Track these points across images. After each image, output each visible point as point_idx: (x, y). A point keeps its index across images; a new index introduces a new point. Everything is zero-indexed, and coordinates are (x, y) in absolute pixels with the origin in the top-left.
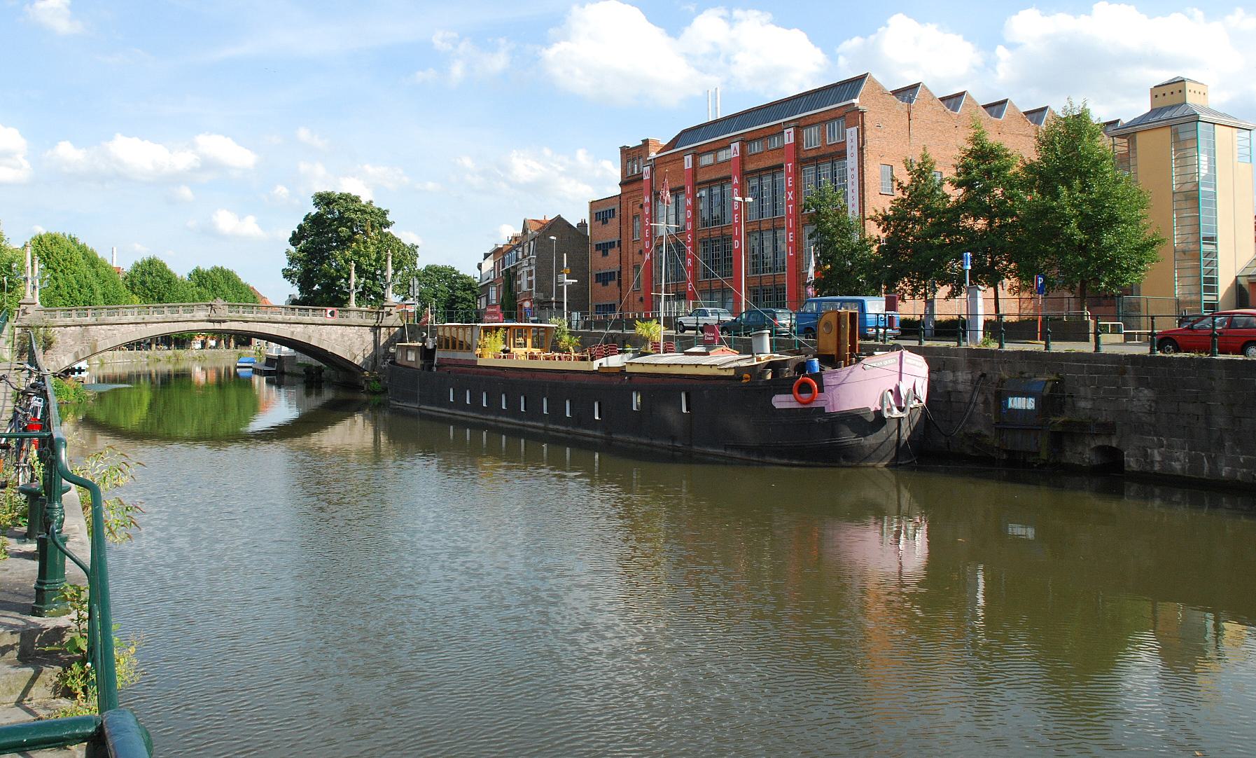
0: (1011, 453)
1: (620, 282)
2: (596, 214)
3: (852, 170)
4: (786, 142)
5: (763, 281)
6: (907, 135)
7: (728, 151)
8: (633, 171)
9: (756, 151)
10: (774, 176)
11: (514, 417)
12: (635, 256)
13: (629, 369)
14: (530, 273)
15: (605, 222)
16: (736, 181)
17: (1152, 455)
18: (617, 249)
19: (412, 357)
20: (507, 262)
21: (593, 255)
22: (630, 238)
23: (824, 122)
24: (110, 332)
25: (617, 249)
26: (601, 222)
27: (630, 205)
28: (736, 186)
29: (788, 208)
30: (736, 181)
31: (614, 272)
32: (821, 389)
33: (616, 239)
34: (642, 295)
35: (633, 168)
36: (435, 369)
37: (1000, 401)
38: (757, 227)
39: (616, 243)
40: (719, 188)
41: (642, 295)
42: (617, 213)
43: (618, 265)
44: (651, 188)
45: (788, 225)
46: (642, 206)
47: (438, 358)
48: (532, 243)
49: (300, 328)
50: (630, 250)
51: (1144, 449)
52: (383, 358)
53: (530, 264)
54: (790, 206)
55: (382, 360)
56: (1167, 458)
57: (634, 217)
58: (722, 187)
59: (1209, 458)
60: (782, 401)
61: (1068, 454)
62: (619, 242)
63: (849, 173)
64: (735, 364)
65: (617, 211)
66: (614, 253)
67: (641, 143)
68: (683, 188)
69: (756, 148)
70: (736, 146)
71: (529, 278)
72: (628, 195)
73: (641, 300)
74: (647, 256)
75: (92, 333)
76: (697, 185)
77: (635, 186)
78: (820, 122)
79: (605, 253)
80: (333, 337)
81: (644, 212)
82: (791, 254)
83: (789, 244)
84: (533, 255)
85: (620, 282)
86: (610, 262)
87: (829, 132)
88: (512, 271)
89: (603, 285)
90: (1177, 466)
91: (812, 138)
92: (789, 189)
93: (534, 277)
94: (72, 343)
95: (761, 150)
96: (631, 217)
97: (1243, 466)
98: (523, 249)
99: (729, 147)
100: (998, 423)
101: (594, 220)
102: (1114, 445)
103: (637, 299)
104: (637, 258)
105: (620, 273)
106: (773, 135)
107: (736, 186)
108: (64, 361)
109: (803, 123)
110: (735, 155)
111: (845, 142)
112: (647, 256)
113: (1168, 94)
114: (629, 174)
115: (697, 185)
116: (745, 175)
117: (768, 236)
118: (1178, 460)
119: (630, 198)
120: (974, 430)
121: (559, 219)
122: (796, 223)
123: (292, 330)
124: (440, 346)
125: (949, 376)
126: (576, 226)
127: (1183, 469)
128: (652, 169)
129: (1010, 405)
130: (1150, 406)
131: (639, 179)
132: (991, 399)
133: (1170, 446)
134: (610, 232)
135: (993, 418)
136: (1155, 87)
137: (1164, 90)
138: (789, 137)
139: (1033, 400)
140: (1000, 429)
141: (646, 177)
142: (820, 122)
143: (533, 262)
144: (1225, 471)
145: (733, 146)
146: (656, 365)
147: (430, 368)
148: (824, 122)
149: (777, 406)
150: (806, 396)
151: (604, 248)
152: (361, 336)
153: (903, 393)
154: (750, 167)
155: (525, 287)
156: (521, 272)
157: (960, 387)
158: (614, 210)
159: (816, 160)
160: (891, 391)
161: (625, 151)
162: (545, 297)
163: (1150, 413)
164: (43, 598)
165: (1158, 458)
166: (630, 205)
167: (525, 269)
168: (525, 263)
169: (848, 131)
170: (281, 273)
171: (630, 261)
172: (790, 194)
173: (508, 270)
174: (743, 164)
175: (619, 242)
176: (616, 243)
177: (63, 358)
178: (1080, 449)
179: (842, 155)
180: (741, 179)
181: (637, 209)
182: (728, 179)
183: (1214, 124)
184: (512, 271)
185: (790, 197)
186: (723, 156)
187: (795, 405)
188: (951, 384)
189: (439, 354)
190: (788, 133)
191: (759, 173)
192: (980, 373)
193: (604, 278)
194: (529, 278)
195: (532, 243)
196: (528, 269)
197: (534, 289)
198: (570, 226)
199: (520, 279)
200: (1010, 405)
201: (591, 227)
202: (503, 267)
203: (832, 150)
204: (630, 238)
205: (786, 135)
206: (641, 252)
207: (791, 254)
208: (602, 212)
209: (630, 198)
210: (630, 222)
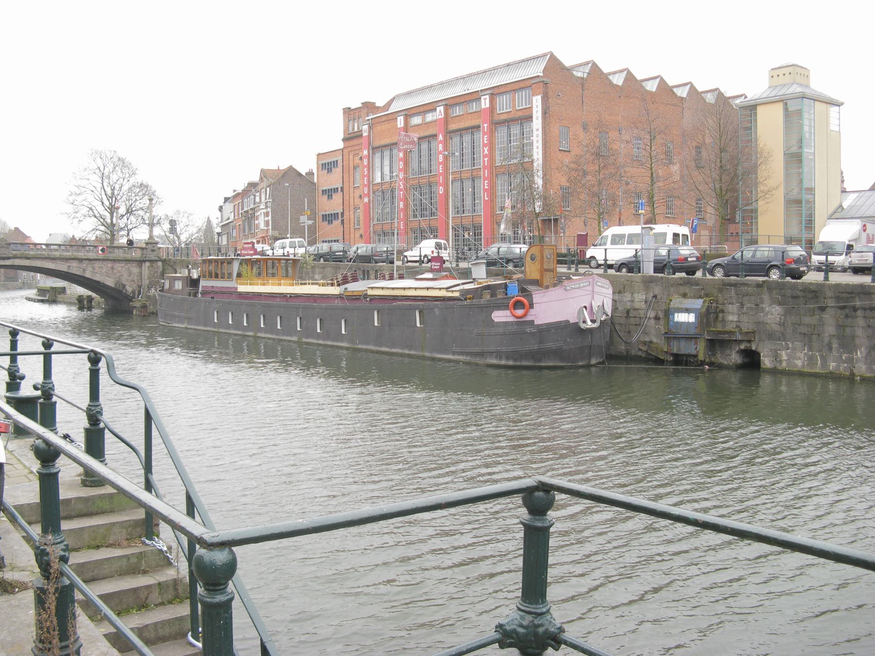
0: (676, 356)
1: (343, 221)
3: (537, 130)
4: (483, 107)
5: (463, 221)
6: (581, 103)
7: (434, 114)
8: (353, 129)
9: (458, 114)
10: (472, 134)
11: (272, 333)
12: (356, 201)
13: (370, 292)
14: (267, 214)
15: (329, 171)
16: (441, 138)
17: (781, 355)
18: (340, 194)
19: (179, 285)
20: (245, 205)
21: (320, 199)
22: (351, 184)
23: (514, 90)
25: (340, 194)
26: (326, 171)
27: (351, 157)
28: (441, 142)
29: (484, 161)
30: (441, 138)
31: (338, 213)
32: (531, 306)
33: (339, 185)
34: (362, 232)
35: (354, 126)
36: (200, 295)
37: (668, 318)
38: (458, 176)
39: (339, 189)
40: (518, 127)
41: (362, 232)
42: (340, 164)
43: (341, 207)
44: (369, 143)
45: (484, 174)
46: (361, 158)
47: (203, 287)
48: (268, 189)
50: (352, 195)
51: (776, 351)
53: (267, 207)
54: (486, 159)
56: (791, 357)
57: (355, 168)
58: (429, 142)
59: (822, 356)
60: (500, 316)
61: (719, 355)
62: (342, 188)
63: (535, 133)
64: (461, 287)
65: (340, 164)
66: (337, 197)
67: (360, 105)
68: (478, 127)
69: (458, 111)
70: (441, 109)
71: (266, 219)
72: (350, 149)
73: (361, 236)
74: (366, 200)
76: (496, 124)
77: (355, 142)
78: (511, 91)
79: (330, 197)
81: (362, 163)
82: (486, 199)
83: (485, 190)
85: (343, 221)
86: (334, 205)
87: (519, 99)
88: (250, 212)
89: (329, 223)
90: (799, 363)
91: (504, 105)
92: (485, 145)
93: (270, 218)
95: (461, 113)
96: (352, 167)
97: (845, 362)
98: (260, 194)
99: (435, 110)
100: (666, 333)
101: (320, 169)
102: (754, 348)
103: (357, 235)
104: (357, 201)
105: (342, 214)
106: (472, 101)
107: (441, 142)
109: (496, 91)
110: (440, 117)
111: (531, 108)
112: (366, 200)
113: (781, 75)
114: (351, 131)
115: (496, 124)
116: (449, 134)
117: (468, 184)
118: (800, 359)
119: (351, 151)
120: (647, 339)
121: (291, 169)
122: (491, 173)
124: (204, 276)
125: (627, 297)
126: (304, 174)
127: (803, 366)
128: (370, 128)
129: (676, 319)
130: (780, 318)
131: (358, 135)
132: (661, 315)
133: (794, 349)
134: (334, 180)
135: (662, 329)
136: (772, 69)
137: (781, 72)
138: (485, 103)
139: (694, 315)
140: (668, 338)
141: (365, 134)
142: (511, 91)
143: (269, 204)
144: (832, 365)
145: (438, 109)
146: (393, 289)
147: (195, 295)
148: (514, 90)
149: (496, 320)
150: (520, 312)
151: (329, 193)
153: (595, 309)
154: (453, 127)
155: (262, 226)
156: (259, 213)
157: (637, 305)
158: (337, 161)
159: (508, 122)
160: (585, 307)
161: (348, 111)
162: (279, 234)
163: (780, 324)
165: (785, 357)
166: (351, 157)
167: (262, 211)
168: (262, 206)
169: (535, 98)
170: (315, 158)
171: (352, 204)
172: (486, 149)
173: (247, 212)
174: (447, 124)
175: (342, 188)
176: (339, 189)
178: (728, 352)
179: (530, 118)
180: (445, 137)
181: (357, 161)
182: (435, 136)
183: (814, 100)
184: (250, 212)
185: (486, 152)
186: (430, 117)
187: (512, 319)
188: (629, 304)
189: (203, 283)
190: (485, 99)
191: (461, 131)
192: (652, 294)
193: (329, 218)
194: (266, 219)
195: (268, 189)
196: (265, 211)
197: (270, 227)
198: (300, 175)
199: (257, 219)
200: (676, 319)
201: (318, 176)
202: (242, 209)
203: (520, 114)
204: (351, 184)
205: (483, 101)
206: (360, 197)
207: (486, 199)
208: (327, 164)
209: (351, 151)
210: (351, 172)
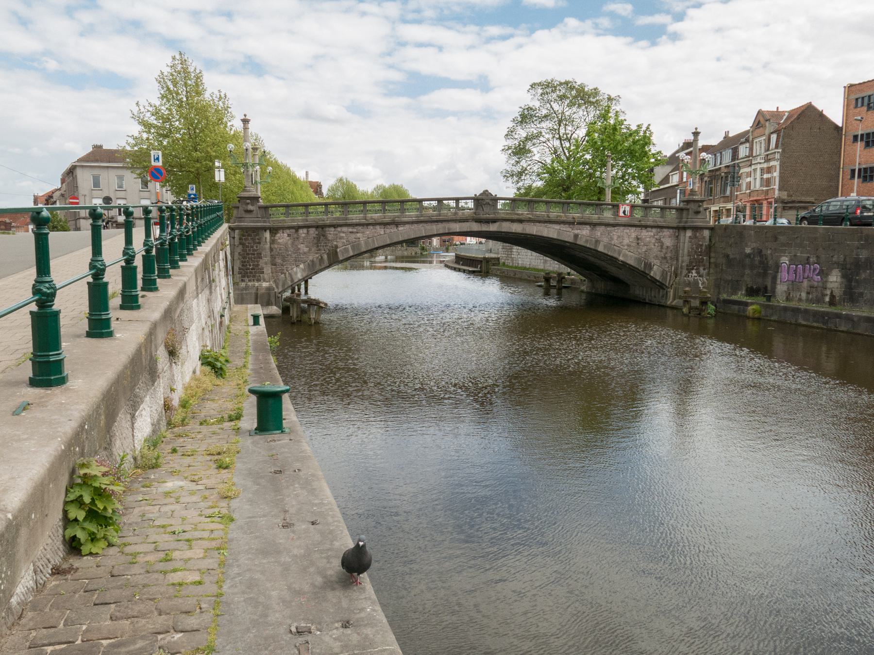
2: (857, 99)
24: (353, 236)
26: (865, 108)
49: (585, 231)
52: (687, 269)
55: (685, 272)
60: (154, 253)
75: (330, 237)
80: (626, 241)
84: (777, 147)
94: (306, 250)
101: (852, 107)
108: (296, 273)
123: (576, 232)
152: (659, 240)
164: (58, 365)
177: (295, 269)
195: (774, 137)
